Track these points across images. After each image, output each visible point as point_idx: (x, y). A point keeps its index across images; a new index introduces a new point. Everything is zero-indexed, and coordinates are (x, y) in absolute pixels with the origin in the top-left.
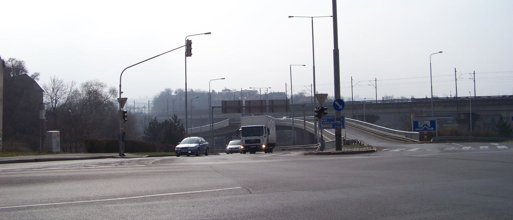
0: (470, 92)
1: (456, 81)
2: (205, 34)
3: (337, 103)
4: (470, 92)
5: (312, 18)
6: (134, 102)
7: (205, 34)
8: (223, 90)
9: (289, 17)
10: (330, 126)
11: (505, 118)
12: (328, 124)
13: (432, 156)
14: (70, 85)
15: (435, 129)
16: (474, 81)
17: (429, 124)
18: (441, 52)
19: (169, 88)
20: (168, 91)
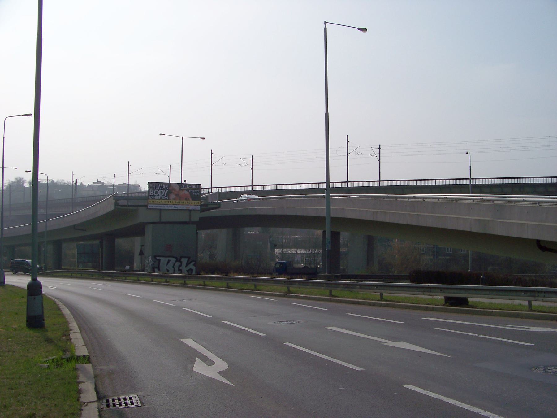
0: (467, 153)
1: (348, 155)
2: (23, 115)
4: (467, 153)
5: (182, 138)
7: (23, 115)
8: (94, 183)
9: (161, 134)
16: (380, 161)
19: (21, 177)
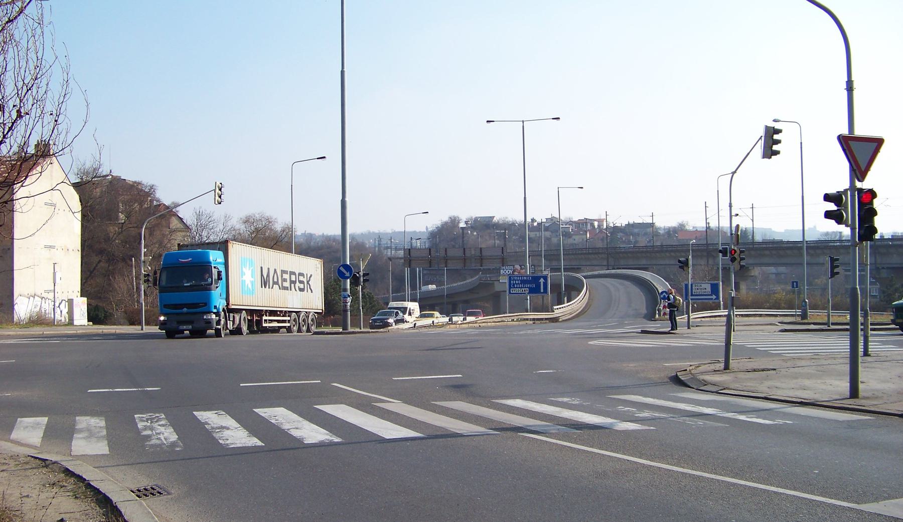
3: (342, 269)
7: (553, 119)
10: (525, 291)
12: (522, 288)
15: (718, 298)
17: (709, 289)
20: (454, 221)
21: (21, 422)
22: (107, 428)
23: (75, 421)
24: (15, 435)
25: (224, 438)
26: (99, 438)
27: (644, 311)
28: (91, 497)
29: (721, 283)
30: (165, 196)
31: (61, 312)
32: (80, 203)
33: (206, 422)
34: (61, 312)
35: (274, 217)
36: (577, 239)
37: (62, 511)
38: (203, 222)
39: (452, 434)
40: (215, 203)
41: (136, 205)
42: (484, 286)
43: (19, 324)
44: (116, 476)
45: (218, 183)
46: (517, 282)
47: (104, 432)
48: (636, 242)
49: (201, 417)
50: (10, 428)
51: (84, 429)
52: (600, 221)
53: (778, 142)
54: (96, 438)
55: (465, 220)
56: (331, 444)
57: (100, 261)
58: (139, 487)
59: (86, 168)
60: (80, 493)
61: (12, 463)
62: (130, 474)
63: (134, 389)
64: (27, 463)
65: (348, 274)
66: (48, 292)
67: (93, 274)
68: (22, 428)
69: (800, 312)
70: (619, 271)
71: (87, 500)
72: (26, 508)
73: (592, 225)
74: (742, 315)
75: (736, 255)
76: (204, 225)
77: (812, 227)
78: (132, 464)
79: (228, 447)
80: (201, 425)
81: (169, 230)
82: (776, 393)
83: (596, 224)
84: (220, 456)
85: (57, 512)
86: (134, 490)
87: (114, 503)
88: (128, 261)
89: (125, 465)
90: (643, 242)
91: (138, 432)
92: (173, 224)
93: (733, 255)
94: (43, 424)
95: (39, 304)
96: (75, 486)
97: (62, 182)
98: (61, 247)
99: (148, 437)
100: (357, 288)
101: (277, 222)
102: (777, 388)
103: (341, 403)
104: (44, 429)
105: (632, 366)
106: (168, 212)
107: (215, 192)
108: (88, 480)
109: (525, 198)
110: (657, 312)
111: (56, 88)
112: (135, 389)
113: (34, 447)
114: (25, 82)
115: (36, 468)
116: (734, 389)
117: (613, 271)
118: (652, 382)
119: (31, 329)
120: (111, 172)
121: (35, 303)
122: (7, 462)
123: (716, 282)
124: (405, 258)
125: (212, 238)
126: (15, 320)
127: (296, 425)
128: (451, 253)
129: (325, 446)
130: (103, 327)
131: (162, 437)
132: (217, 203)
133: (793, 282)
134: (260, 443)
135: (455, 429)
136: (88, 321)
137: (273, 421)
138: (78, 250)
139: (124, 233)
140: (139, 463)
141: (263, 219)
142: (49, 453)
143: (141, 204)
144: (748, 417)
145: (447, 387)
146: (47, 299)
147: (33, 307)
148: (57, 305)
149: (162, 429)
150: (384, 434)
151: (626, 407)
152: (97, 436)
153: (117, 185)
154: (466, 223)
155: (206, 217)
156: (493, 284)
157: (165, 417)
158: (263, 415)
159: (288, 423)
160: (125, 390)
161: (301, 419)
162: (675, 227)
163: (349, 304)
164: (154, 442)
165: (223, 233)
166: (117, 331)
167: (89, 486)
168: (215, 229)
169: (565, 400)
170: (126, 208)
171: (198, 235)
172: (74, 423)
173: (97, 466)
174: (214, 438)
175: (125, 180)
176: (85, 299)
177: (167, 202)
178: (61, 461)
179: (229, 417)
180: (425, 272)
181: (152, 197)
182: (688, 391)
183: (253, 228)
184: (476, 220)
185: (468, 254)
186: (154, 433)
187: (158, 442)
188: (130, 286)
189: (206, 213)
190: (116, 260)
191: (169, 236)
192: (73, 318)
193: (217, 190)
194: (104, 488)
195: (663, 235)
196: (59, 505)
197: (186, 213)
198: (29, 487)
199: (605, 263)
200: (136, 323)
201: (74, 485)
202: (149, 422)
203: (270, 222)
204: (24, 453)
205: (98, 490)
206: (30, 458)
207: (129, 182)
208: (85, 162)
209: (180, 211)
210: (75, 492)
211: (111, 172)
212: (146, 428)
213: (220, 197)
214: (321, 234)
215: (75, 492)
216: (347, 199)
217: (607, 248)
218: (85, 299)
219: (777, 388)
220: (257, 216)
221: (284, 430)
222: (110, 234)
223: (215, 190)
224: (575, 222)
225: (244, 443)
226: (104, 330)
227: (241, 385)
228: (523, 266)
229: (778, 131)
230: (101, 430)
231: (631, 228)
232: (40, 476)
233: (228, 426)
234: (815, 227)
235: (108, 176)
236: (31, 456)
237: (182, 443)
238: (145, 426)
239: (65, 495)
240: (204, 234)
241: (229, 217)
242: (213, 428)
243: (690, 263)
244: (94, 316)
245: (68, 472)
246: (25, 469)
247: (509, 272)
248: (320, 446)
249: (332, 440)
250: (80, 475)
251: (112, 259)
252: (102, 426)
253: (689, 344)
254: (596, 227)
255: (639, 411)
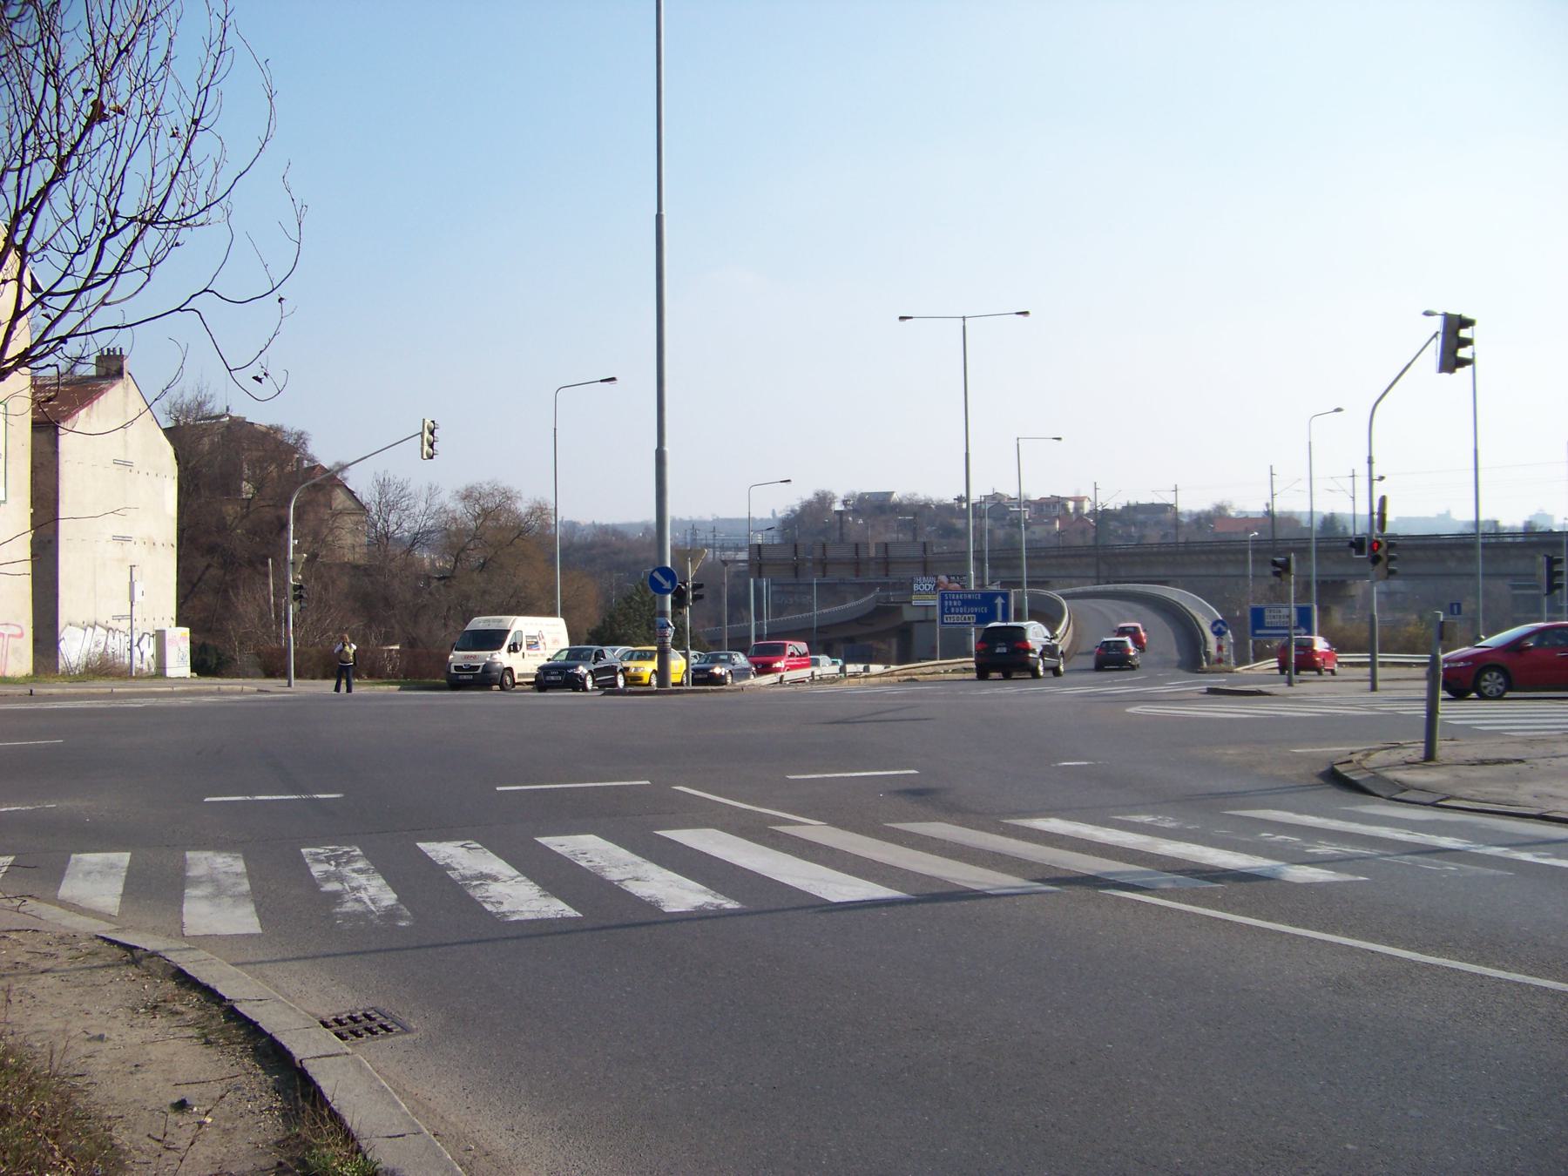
2: (602, 381)
3: (657, 575)
5: (964, 320)
6: (714, 531)
7: (602, 381)
9: (902, 318)
10: (969, 618)
11: (1456, 612)
12: (964, 613)
13: (210, 702)
14: (424, 495)
18: (1338, 410)
20: (823, 500)
21: (78, 861)
22: (250, 875)
23: (184, 860)
24: (67, 890)
25: (492, 900)
26: (238, 898)
27: (1175, 656)
28: (240, 1043)
29: (1315, 607)
30: (323, 452)
31: (142, 654)
32: (175, 462)
33: (448, 864)
34: (142, 654)
35: (516, 489)
36: (1039, 531)
37: (181, 1077)
38: (391, 497)
39: (961, 892)
40: (422, 457)
41: (273, 467)
42: (883, 611)
43: (70, 676)
44: (284, 985)
45: (428, 421)
46: (955, 604)
47: (245, 886)
48: (1142, 537)
49: (434, 853)
50: (57, 874)
51: (204, 879)
52: (1079, 501)
53: (1467, 342)
54: (231, 897)
55: (843, 498)
56: (720, 914)
57: (209, 566)
58: (336, 1012)
59: (185, 401)
60: (216, 1030)
61: (64, 953)
62: (314, 982)
63: (292, 797)
64: (94, 954)
65: (667, 585)
66: (119, 618)
67: (196, 589)
68: (80, 876)
69: (1367, 657)
70: (1120, 587)
71: (234, 1050)
72: (98, 1066)
73: (1065, 507)
74: (1351, 664)
75: (1380, 552)
76: (391, 504)
77: (1444, 512)
78: (315, 957)
79: (506, 920)
80: (439, 872)
81: (329, 511)
82: (1558, 806)
83: (1071, 505)
84: (494, 940)
85: (168, 1080)
86: (329, 1020)
87: (297, 1061)
88: (259, 567)
89: (298, 959)
90: (1153, 536)
91: (314, 885)
92: (338, 501)
93: (1374, 551)
94: (122, 868)
95: (103, 639)
96: (200, 1013)
97: (205, 290)
98: (142, 539)
99: (336, 897)
100: (681, 610)
101: (521, 498)
102: (1551, 796)
103: (708, 826)
104: (124, 878)
105: (1232, 755)
106: (328, 481)
107: (422, 437)
108: (229, 1000)
109: (967, 454)
110: (1204, 658)
111: (188, 67)
112: (296, 797)
113: (106, 917)
114: (112, 30)
115: (113, 966)
116: (1466, 799)
117: (1111, 587)
118: (1293, 785)
119: (89, 683)
120: (228, 409)
121: (96, 638)
122: (52, 950)
123: (1305, 605)
124: (750, 561)
125: (406, 525)
126: (60, 667)
127: (628, 872)
128: (832, 553)
129: (707, 918)
130: (218, 680)
131: (363, 895)
132: (425, 457)
133: (1452, 605)
134: (570, 912)
135: (965, 881)
136: (191, 672)
137: (583, 863)
138: (173, 545)
139: (251, 516)
140: (328, 956)
141: (496, 493)
142: (137, 929)
143: (281, 467)
144: (1538, 857)
145: (899, 792)
146: (118, 632)
147: (93, 645)
148: (135, 642)
149: (361, 880)
150: (823, 891)
151: (1276, 834)
152: (230, 893)
153: (238, 431)
154: (845, 502)
155: (396, 490)
156: (900, 608)
157: (361, 853)
158: (559, 850)
159: (616, 867)
160: (274, 797)
161: (638, 859)
162: (1209, 512)
163: (670, 639)
164: (350, 906)
165: (425, 517)
166: (245, 687)
167: (232, 1014)
168: (413, 511)
169: (1147, 819)
170: (255, 472)
171: (381, 521)
172: (183, 866)
173: (240, 960)
174: (472, 900)
175: (252, 423)
176: (186, 631)
177: (327, 462)
178: (166, 950)
179: (489, 854)
180: (775, 588)
181: (301, 453)
182: (1373, 803)
183: (478, 508)
184: (862, 498)
185: (863, 555)
186: (347, 888)
187: (358, 907)
188: (266, 608)
189: (396, 481)
190: (237, 565)
191: (330, 522)
192: (165, 664)
193: (427, 434)
194: (270, 1019)
195: (1188, 525)
196: (172, 1061)
197: (361, 482)
198: (102, 1013)
199: (1092, 573)
200: (277, 674)
201: (199, 1009)
202: (333, 863)
203: (508, 498)
204: (88, 930)
205: (255, 1024)
206: (99, 941)
207: (260, 428)
208: (183, 392)
209: (350, 478)
210: (203, 1028)
211: (228, 409)
212: (328, 877)
213: (431, 446)
214: (589, 522)
215: (203, 1028)
216: (667, 448)
217: (1095, 547)
218: (186, 631)
219: (1551, 796)
220: (486, 487)
221: (611, 882)
222: (228, 518)
223: (422, 434)
224: (1034, 502)
225: (539, 912)
226: (221, 687)
227: (498, 789)
228: (962, 576)
229: (1467, 323)
230: (238, 881)
231: (1132, 513)
232: (121, 986)
233: (494, 873)
234: (1448, 512)
235: (223, 416)
236: (102, 938)
237: (408, 909)
238: (326, 872)
239: (182, 1034)
240: (393, 518)
241: (436, 489)
242: (464, 878)
243: (1293, 566)
244: (200, 665)
245: (184, 979)
246: (90, 968)
247: (928, 587)
248: (700, 918)
249: (720, 905)
250: (212, 985)
251: (230, 562)
252: (239, 870)
253: (1310, 712)
254: (1071, 511)
255: (1307, 842)
